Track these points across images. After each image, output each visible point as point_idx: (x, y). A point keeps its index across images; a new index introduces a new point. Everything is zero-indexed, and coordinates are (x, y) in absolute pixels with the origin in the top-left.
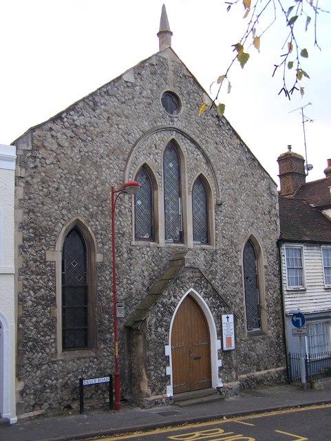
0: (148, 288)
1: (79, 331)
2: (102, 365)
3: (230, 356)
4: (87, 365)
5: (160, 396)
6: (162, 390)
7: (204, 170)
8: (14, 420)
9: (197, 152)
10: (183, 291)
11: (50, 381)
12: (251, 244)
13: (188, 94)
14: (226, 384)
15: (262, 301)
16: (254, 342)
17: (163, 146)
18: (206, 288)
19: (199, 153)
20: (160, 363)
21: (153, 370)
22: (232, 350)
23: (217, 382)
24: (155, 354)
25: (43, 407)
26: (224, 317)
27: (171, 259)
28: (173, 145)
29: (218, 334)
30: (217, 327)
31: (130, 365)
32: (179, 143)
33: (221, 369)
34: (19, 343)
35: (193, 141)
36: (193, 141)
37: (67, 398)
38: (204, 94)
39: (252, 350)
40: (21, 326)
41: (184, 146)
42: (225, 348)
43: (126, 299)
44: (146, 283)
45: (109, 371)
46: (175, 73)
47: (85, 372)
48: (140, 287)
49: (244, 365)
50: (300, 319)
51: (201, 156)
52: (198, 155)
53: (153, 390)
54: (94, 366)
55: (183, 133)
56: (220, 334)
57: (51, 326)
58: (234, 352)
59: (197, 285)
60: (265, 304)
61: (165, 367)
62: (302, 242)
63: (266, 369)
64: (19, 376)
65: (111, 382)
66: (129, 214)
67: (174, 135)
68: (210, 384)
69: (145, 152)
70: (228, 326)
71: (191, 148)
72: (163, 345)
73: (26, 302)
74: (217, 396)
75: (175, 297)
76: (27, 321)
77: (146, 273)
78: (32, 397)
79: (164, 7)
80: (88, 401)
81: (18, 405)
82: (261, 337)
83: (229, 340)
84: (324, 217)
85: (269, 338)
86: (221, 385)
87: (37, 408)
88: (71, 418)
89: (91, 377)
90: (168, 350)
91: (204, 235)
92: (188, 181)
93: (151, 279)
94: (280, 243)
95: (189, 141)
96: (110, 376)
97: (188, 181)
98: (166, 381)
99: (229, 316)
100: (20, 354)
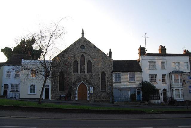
1: (62, 88)
6: (75, 99)
7: (90, 59)
9: (88, 56)
12: (103, 74)
16: (103, 93)
23: (88, 99)
28: (83, 56)
34: (52, 89)
41: (85, 55)
55: (86, 53)
56: (89, 90)
57: (57, 87)
60: (106, 85)
62: (120, 72)
64: (51, 94)
70: (91, 89)
79: (110, 50)
90: (77, 92)
91: (89, 71)
92: (86, 62)
94: (112, 72)
97: (86, 62)
100: (52, 91)
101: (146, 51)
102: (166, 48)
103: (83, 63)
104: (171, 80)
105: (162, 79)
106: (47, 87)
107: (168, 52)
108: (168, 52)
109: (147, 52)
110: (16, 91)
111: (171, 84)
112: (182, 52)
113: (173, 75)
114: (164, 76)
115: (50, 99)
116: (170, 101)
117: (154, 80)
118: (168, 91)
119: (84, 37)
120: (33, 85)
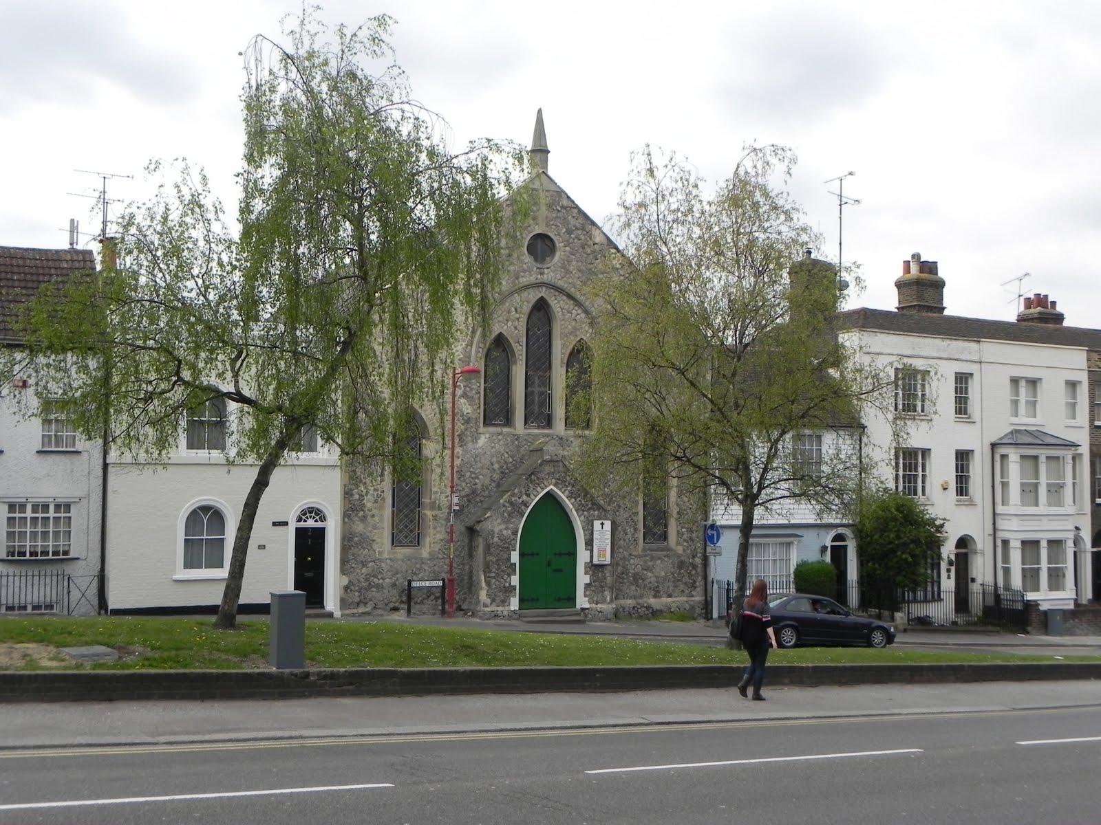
0: (499, 483)
2: (436, 568)
3: (603, 572)
4: (418, 566)
5: (500, 609)
6: (504, 602)
8: (337, 614)
9: (577, 311)
10: (539, 489)
11: (375, 580)
13: (569, 232)
14: (594, 606)
15: (671, 506)
17: (527, 308)
18: (573, 486)
19: (580, 311)
20: (503, 571)
21: (494, 578)
22: (606, 565)
23: (582, 601)
24: (497, 560)
25: (368, 606)
26: (597, 524)
27: (531, 449)
28: (541, 307)
29: (586, 544)
30: (585, 535)
31: (471, 572)
32: (550, 301)
33: (587, 586)
35: (570, 297)
36: (570, 297)
37: (394, 599)
38: (594, 228)
39: (648, 569)
40: (346, 520)
41: (558, 305)
42: (596, 561)
43: (467, 496)
44: (496, 476)
45: (444, 575)
46: (550, 206)
47: (415, 574)
48: (487, 482)
49: (633, 588)
50: (715, 533)
51: (583, 315)
52: (578, 314)
53: (493, 601)
54: (426, 568)
55: (560, 290)
56: (589, 543)
58: (609, 568)
59: (560, 482)
61: (509, 575)
63: (670, 596)
64: (343, 571)
65: (444, 587)
66: (477, 396)
67: (543, 293)
68: (572, 599)
69: (500, 319)
71: (566, 307)
72: (508, 550)
73: (352, 495)
74: (581, 618)
75: (528, 495)
76: (353, 515)
77: (496, 466)
78: (357, 594)
79: (540, 112)
80: (418, 606)
81: (343, 601)
82: (665, 553)
83: (603, 551)
84: (306, 558)
85: (679, 556)
86: (587, 606)
87: (362, 605)
88: (400, 616)
89: (422, 580)
90: (515, 557)
93: (502, 472)
95: (565, 298)
96: (443, 580)
98: (511, 592)
99: (604, 522)
101: (1046, 296)
102: (942, 273)
103: (539, 362)
104: (998, 488)
105: (954, 474)
106: (310, 523)
107: (955, 304)
108: (955, 304)
109: (851, 302)
110: (55, 553)
111: (1000, 509)
112: (1009, 313)
113: (1014, 456)
114: (963, 457)
115: (331, 602)
116: (987, 610)
117: (916, 482)
118: (983, 553)
119: (550, 173)
120: (205, 509)
